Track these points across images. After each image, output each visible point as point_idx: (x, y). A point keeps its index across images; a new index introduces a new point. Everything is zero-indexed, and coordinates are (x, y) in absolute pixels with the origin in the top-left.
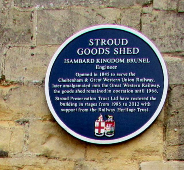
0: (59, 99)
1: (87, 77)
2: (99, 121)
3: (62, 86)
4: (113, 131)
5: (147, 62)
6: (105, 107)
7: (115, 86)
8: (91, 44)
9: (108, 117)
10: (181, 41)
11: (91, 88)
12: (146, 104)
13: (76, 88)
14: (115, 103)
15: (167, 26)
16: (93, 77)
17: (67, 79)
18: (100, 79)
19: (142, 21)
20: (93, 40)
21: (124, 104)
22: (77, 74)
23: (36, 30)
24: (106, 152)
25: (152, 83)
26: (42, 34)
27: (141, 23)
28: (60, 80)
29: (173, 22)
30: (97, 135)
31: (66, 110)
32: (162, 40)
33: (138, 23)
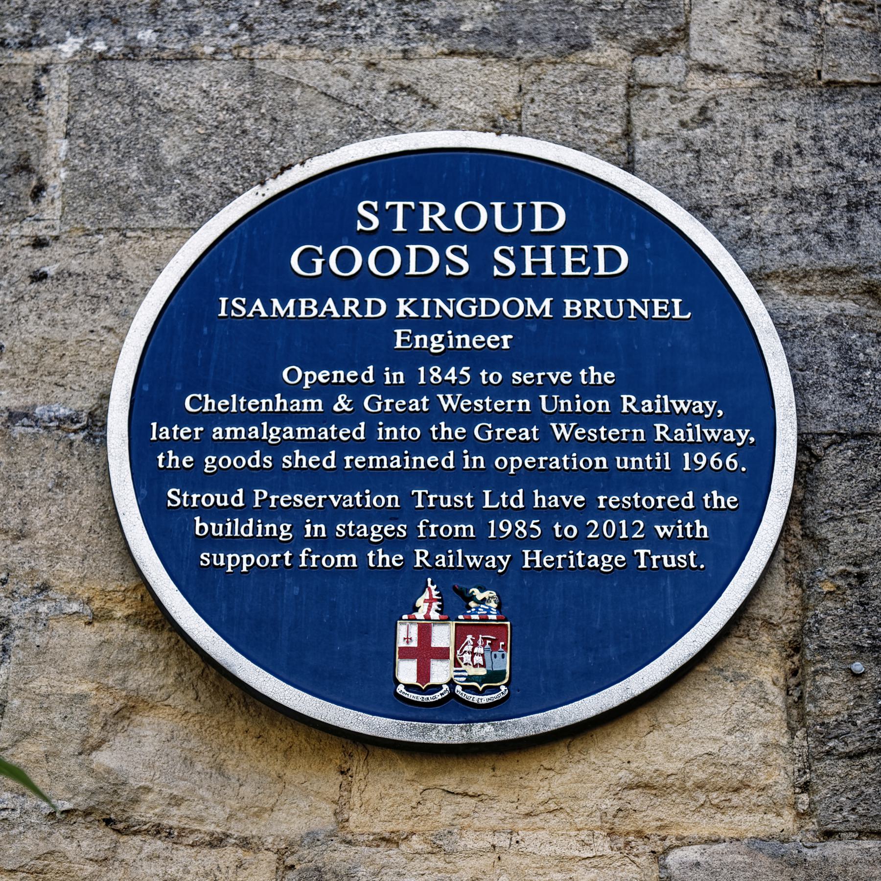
0: (190, 499)
1: (344, 387)
2: (420, 615)
3: (206, 434)
4: (504, 672)
5: (677, 315)
6: (455, 542)
7: (503, 433)
8: (367, 222)
9: (473, 598)
10: (851, 221)
11: (370, 446)
12: (684, 529)
13: (287, 446)
14: (505, 525)
15: (767, 149)
16: (378, 386)
17: (234, 396)
18: (419, 399)
19: (635, 120)
20: (375, 204)
21: (561, 530)
22: (292, 374)
23: (62, 154)
24: (465, 794)
25: (712, 422)
26: (92, 175)
27: (627, 134)
28: (195, 402)
29: (800, 124)
30: (412, 696)
31: (228, 561)
32: (746, 213)
33: (616, 129)
